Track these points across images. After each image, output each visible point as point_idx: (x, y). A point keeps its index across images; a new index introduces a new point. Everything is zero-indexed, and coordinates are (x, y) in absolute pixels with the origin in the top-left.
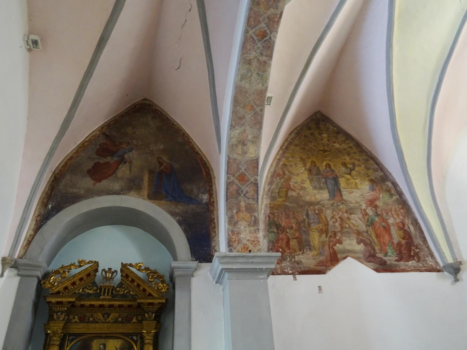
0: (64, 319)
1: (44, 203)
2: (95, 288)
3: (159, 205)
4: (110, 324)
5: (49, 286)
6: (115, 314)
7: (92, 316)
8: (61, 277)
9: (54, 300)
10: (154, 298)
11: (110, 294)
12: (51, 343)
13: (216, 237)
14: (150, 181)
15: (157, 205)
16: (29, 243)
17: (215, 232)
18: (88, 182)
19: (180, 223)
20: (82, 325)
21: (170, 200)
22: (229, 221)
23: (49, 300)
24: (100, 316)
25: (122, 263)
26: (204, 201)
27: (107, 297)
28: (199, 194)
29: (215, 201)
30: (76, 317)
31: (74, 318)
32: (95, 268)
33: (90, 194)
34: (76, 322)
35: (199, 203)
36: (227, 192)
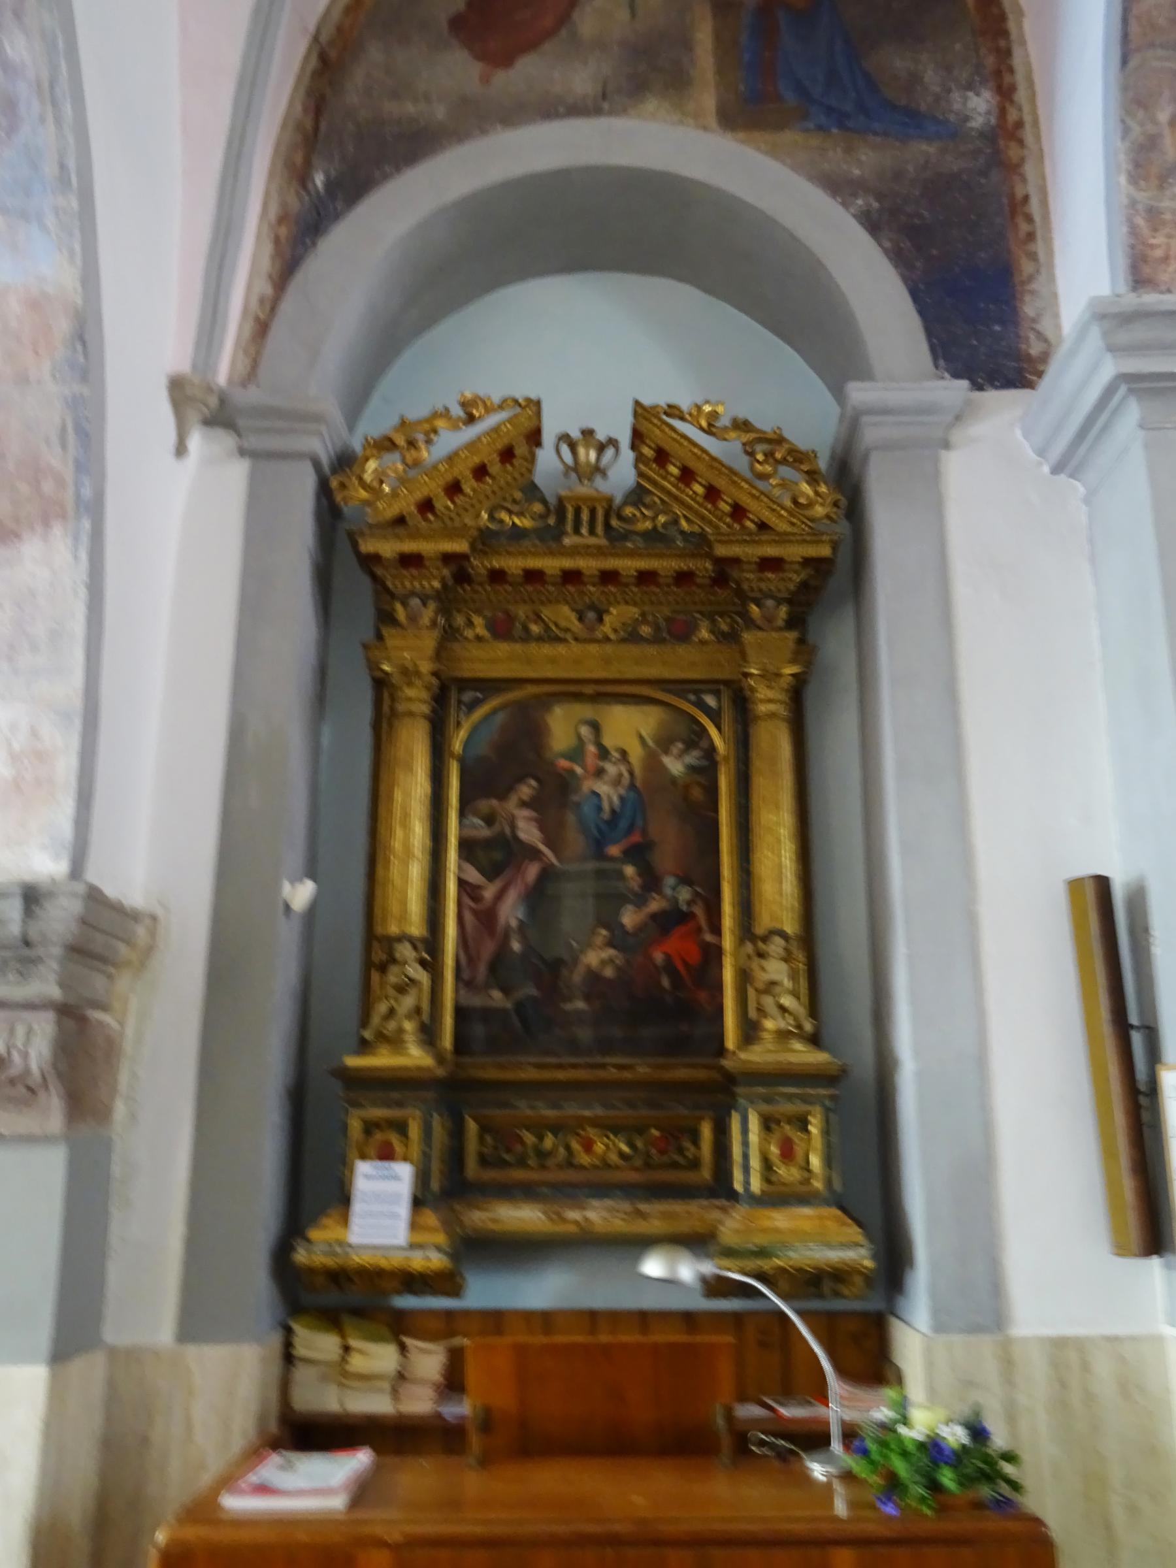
0: (434, 623)
1: (295, 166)
2: (538, 507)
3: (774, 152)
4: (609, 648)
5: (363, 494)
6: (624, 608)
7: (538, 618)
8: (404, 462)
9: (388, 548)
10: (783, 539)
11: (600, 529)
12: (401, 707)
13: (1042, 278)
14: (724, 46)
15: (766, 153)
16: (261, 329)
17: (1033, 257)
18: (456, 71)
19: (872, 225)
20: (503, 648)
21: (820, 128)
22: (1137, 165)
23: (368, 546)
24: (565, 615)
25: (637, 403)
26: (977, 122)
27: (592, 541)
28: (949, 91)
29: (1027, 118)
30: (478, 621)
31: (470, 624)
32: (527, 425)
33: (474, 118)
34: (479, 639)
35: (952, 132)
36: (1125, 20)
